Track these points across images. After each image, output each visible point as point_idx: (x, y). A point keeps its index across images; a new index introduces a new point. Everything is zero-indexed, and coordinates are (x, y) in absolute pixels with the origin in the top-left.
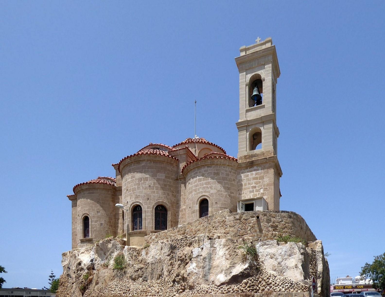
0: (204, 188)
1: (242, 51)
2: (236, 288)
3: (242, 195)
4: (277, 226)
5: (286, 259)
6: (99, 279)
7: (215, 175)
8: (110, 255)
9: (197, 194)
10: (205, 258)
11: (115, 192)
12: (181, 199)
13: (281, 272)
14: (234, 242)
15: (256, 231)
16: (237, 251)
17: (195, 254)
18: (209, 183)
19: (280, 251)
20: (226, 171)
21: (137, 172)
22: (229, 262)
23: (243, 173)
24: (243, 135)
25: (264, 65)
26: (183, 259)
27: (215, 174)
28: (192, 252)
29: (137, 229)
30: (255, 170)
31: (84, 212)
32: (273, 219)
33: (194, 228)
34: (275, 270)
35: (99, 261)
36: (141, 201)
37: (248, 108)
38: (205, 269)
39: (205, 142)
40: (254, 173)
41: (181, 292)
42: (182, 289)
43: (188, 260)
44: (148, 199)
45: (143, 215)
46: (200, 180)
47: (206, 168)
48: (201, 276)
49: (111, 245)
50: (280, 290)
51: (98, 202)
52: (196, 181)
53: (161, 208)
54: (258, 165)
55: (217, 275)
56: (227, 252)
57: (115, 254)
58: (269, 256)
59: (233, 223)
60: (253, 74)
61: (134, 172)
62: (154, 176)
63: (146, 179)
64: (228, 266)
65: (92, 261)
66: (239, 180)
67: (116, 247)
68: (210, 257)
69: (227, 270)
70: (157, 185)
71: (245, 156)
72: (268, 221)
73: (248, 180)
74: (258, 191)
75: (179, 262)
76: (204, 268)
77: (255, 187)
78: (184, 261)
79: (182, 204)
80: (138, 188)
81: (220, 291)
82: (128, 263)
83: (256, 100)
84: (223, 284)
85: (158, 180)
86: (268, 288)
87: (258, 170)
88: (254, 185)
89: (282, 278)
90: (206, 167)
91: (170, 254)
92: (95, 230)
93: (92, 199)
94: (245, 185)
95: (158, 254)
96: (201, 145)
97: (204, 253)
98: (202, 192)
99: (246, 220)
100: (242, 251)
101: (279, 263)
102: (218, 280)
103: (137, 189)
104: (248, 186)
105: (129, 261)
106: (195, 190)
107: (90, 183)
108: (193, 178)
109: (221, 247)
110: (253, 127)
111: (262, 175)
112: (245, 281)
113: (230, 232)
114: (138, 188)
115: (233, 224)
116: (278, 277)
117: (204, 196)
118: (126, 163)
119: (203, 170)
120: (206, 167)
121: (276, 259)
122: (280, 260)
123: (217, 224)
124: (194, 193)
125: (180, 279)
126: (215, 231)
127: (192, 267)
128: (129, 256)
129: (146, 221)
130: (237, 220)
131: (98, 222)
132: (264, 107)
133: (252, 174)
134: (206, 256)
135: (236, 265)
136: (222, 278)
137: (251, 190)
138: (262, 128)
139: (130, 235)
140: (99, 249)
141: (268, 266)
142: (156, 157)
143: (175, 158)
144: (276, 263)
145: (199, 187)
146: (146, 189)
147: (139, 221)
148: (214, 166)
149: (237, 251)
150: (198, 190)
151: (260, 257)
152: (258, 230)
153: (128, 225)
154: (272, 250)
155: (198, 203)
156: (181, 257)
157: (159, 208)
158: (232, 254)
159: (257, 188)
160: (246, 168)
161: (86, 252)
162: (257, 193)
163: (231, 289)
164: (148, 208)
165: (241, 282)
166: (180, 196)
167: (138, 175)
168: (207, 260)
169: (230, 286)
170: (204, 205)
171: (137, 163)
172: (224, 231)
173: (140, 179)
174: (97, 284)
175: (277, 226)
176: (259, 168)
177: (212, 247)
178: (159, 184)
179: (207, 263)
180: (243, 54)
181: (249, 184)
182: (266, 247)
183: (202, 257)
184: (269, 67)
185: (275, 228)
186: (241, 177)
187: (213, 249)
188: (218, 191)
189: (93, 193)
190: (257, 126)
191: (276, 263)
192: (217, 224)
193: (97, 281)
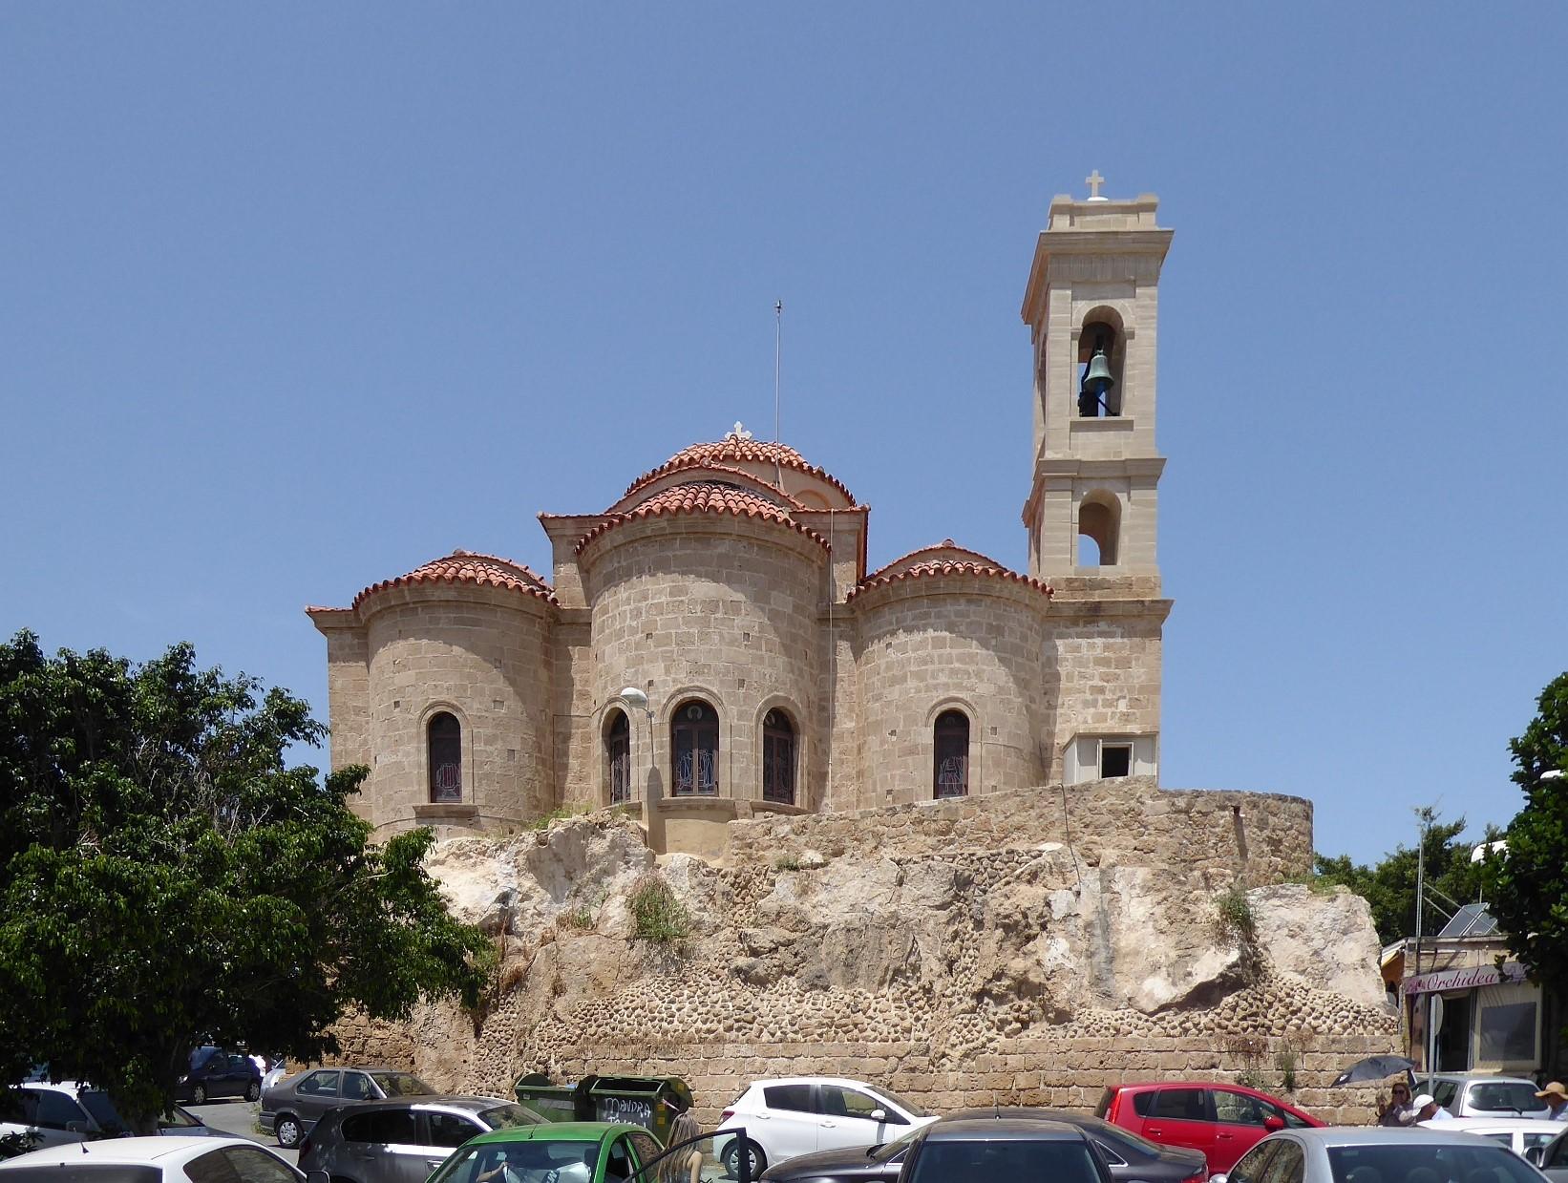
0: (953, 672)
1: (1059, 210)
2: (1204, 1020)
3: (1059, 711)
4: (1280, 841)
5: (1334, 942)
6: (563, 975)
7: (992, 636)
8: (597, 881)
9: (928, 689)
10: (1089, 925)
11: (559, 629)
12: (839, 694)
13: (1322, 978)
14: (1179, 882)
15: (1229, 852)
16: (1193, 908)
17: (1059, 910)
18: (971, 659)
19: (1317, 919)
20: (1021, 624)
21: (699, 575)
22: (1171, 941)
23: (1061, 636)
24: (1061, 506)
25: (1134, 284)
26: (1017, 923)
27: (991, 628)
28: (1048, 904)
29: (689, 789)
30: (1101, 634)
31: (434, 698)
32: (1272, 820)
33: (996, 820)
34: (1303, 972)
35: (542, 901)
36: (711, 687)
37: (1077, 417)
38: (1095, 960)
39: (800, 465)
40: (1099, 641)
41: (1018, 1031)
42: (1017, 1020)
43: (1036, 929)
44: (741, 683)
45: (724, 742)
46: (939, 643)
47: (962, 606)
48: (1085, 982)
49: (606, 843)
50: (1330, 1029)
51: (498, 663)
52: (922, 644)
53: (700, 715)
54: (1113, 619)
55: (1140, 978)
56: (1159, 910)
57: (625, 879)
58: (1286, 931)
59: (1166, 822)
60: (1097, 304)
61: (683, 573)
62: (759, 598)
63: (734, 607)
64: (1173, 954)
65: (504, 898)
66: (1049, 658)
67: (626, 854)
68: (1103, 924)
69: (1172, 965)
70: (772, 636)
71: (1069, 581)
72: (1262, 825)
73: (1080, 662)
74: (1111, 705)
75: (999, 933)
76: (1091, 955)
77: (1101, 690)
78: (1020, 931)
79: (840, 709)
80: (704, 636)
81: (1157, 1029)
82: (695, 918)
83: (1098, 398)
84: (1164, 1008)
85: (774, 616)
86: (1295, 1021)
87: (1112, 635)
88: (1097, 682)
89: (1326, 994)
90: (962, 601)
91: (951, 903)
92: (487, 776)
93: (471, 648)
94: (1070, 677)
95: (879, 900)
96: (798, 475)
97: (1086, 909)
98: (946, 686)
99: (1205, 815)
100: (1209, 909)
101: (1316, 953)
102: (1150, 995)
103: (660, 640)
104: (1076, 683)
105: (699, 909)
106: (920, 676)
107: (425, 577)
108: (909, 630)
109: (1134, 892)
110: (1095, 486)
111: (1125, 653)
112: (1229, 999)
113: (1159, 849)
114: (704, 636)
115: (1167, 825)
116: (1314, 991)
117: (956, 700)
118: (649, 532)
119: (950, 609)
120: (962, 601)
121: (1308, 940)
122: (1318, 943)
123: (1107, 818)
124: (911, 684)
125: (1008, 988)
126: (1095, 838)
127: (1055, 950)
128: (700, 891)
129: (735, 766)
130: (1180, 812)
131: (499, 745)
132: (1128, 425)
133: (1093, 646)
134: (1093, 917)
135: (1199, 952)
136: (1160, 989)
137: (1088, 696)
138: (1122, 497)
139: (662, 811)
140: (545, 856)
141: (1283, 959)
142: (772, 529)
143: (818, 538)
144: (1305, 952)
145: (937, 666)
146: (732, 642)
147: (701, 763)
148: (989, 601)
149: (1193, 908)
150: (933, 677)
151: (1260, 931)
152: (1236, 850)
153: (654, 775)
154: (1295, 914)
155: (932, 721)
156: (1007, 917)
157: (695, 712)
158: (1178, 917)
159: (1109, 696)
160: (1074, 621)
161: (451, 860)
162: (1109, 711)
163: (1189, 1025)
164: (741, 716)
165: (1217, 1004)
166: (834, 684)
167: (702, 589)
168: (1098, 932)
169: (1186, 1014)
170: (952, 731)
171: (697, 540)
172: (1135, 843)
173: (712, 605)
174: (558, 990)
175: (1280, 841)
176: (1113, 628)
177: (1106, 889)
178: (776, 630)
179: (1098, 941)
180: (1062, 224)
181: (1082, 676)
182: (1275, 902)
183: (1080, 922)
184: (1151, 298)
185: (1275, 844)
186: (1055, 647)
187: (1108, 895)
188: (1001, 689)
189: (476, 623)
190: (1107, 486)
191: (1305, 952)
192: (1107, 818)
193: (558, 979)
